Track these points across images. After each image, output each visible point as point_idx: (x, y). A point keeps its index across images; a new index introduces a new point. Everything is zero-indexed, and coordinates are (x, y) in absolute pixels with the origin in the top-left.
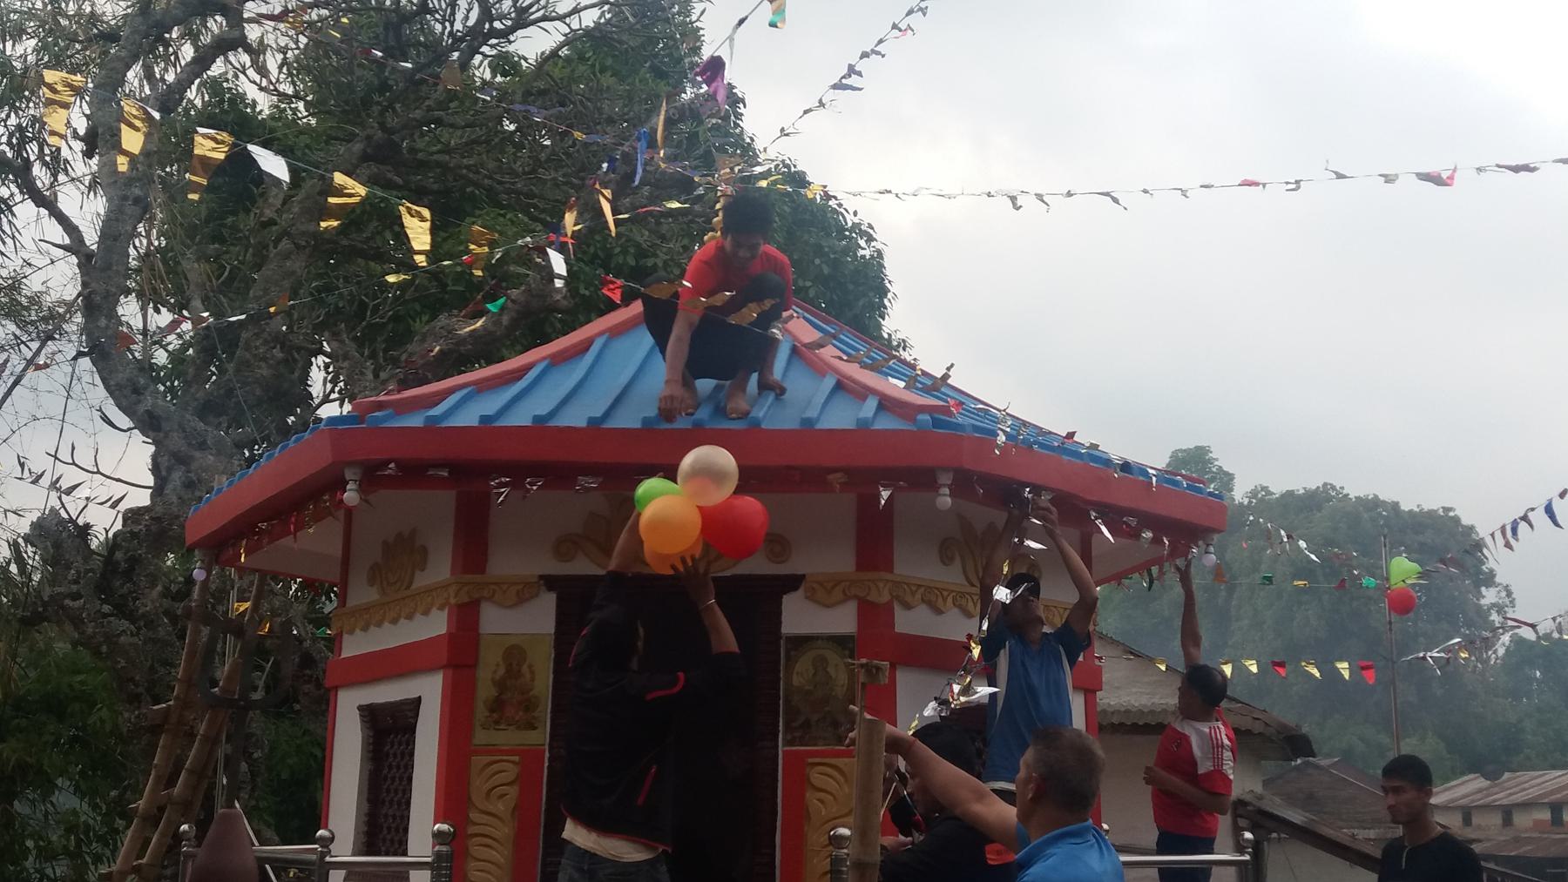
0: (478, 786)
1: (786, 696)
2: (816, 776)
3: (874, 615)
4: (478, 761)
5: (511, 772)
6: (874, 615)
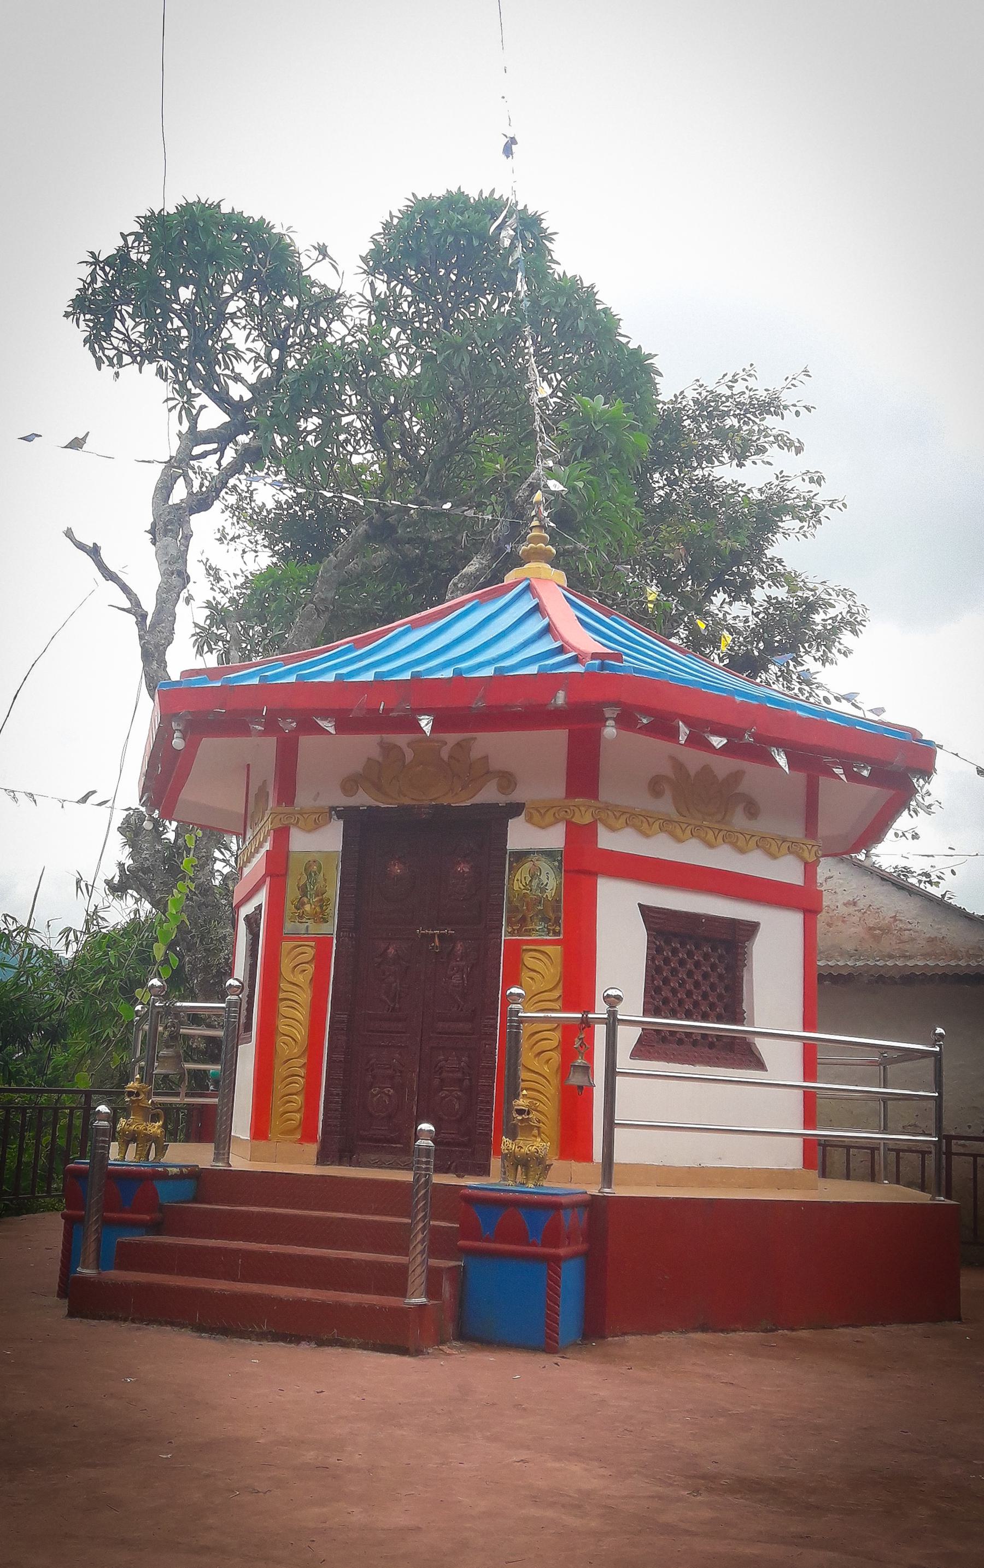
0: (286, 965)
1: (508, 898)
2: (528, 959)
3: (580, 837)
4: (286, 946)
5: (310, 953)
6: (580, 837)
